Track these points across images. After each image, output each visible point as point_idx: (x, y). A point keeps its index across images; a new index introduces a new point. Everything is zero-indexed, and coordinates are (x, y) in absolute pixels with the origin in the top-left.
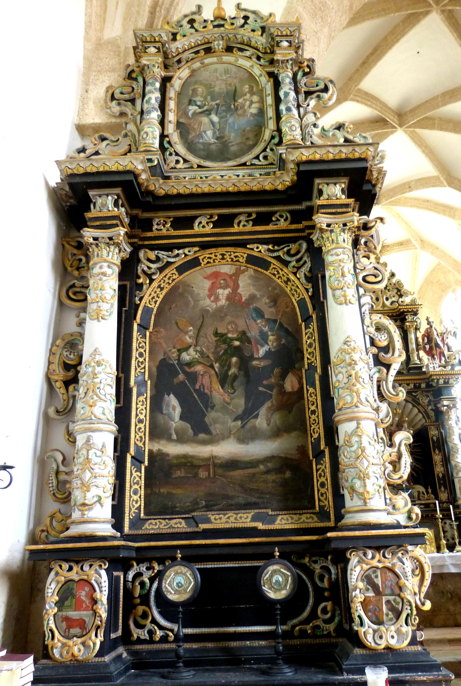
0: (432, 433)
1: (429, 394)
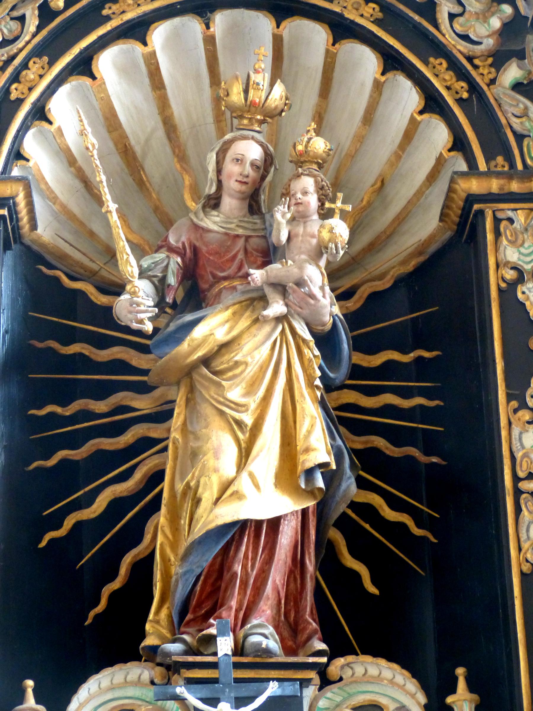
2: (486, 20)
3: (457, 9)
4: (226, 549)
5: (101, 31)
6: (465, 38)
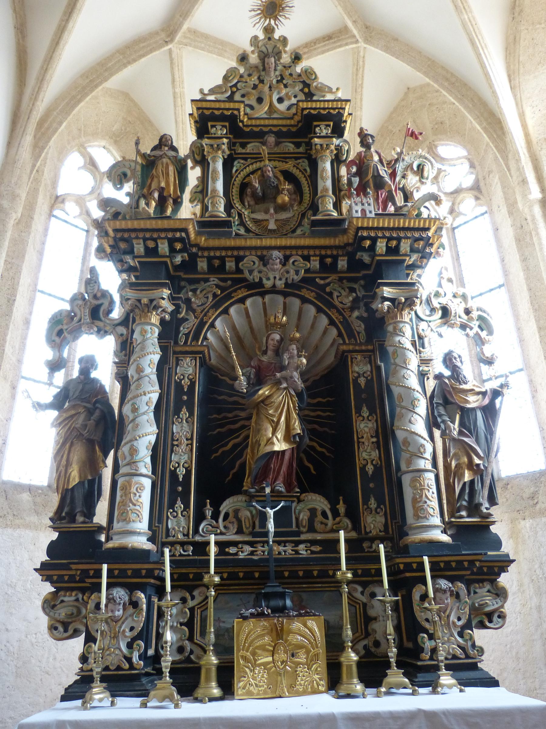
0: (356, 369)
1: (356, 286)
2: (348, 298)
3: (339, 294)
4: (268, 460)
5: (231, 301)
6: (342, 303)
